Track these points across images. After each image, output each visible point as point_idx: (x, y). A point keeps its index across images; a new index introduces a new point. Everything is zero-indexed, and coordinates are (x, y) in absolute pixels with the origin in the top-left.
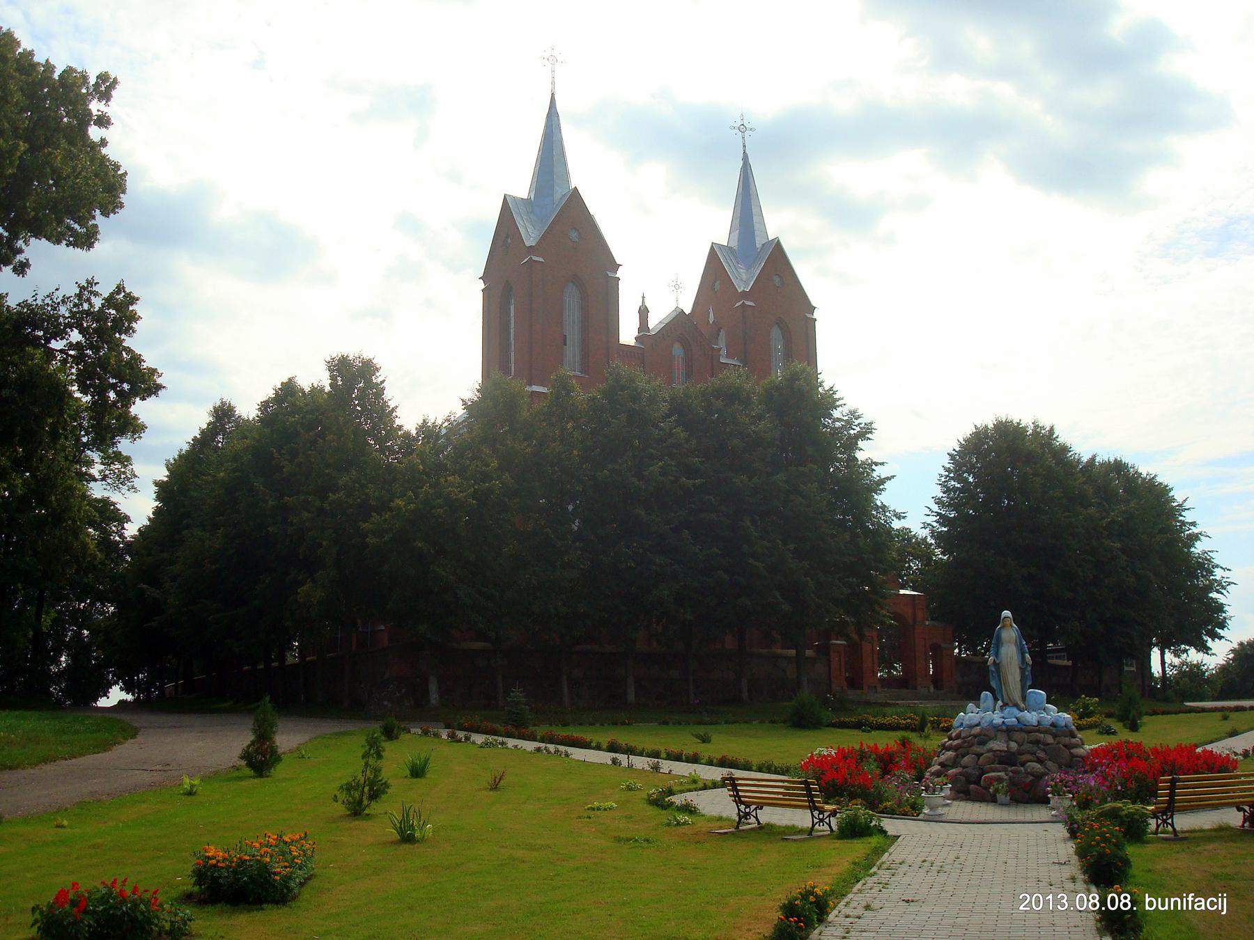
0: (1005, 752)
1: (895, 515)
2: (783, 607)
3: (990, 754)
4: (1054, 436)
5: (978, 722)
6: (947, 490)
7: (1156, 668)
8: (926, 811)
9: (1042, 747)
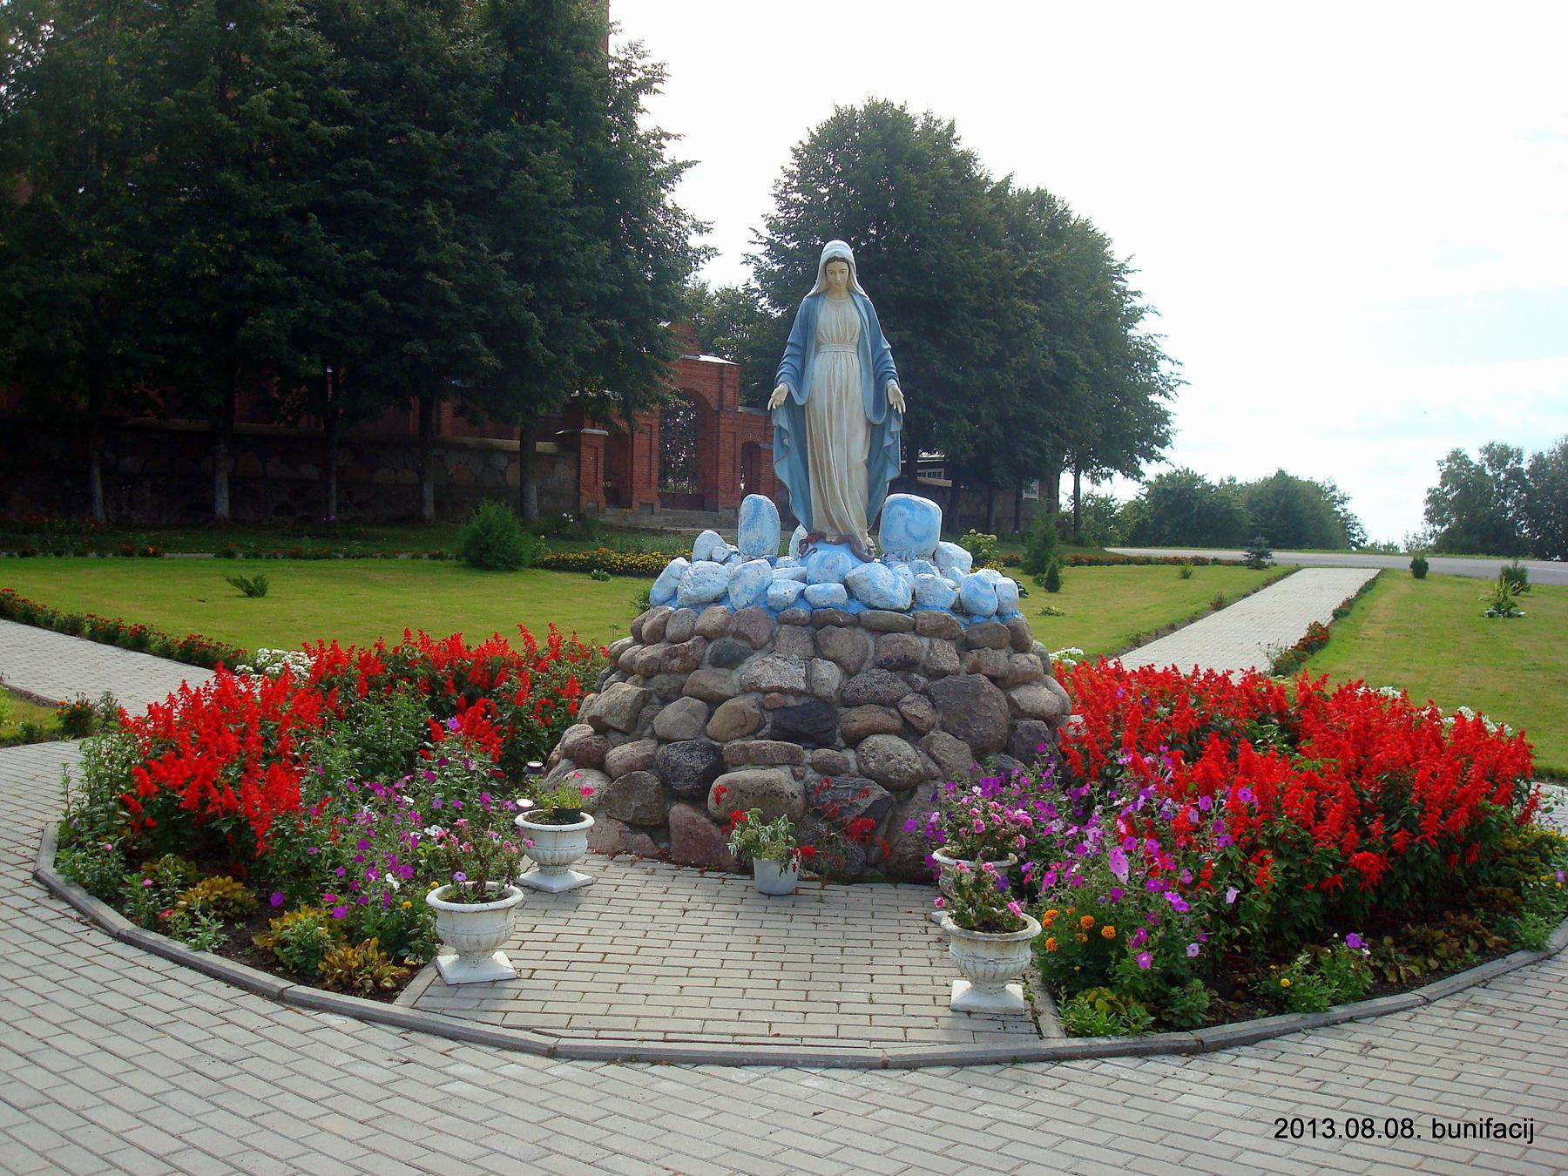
0: (798, 693)
1: (693, 226)
2: (485, 359)
3: (746, 702)
4: (955, 137)
5: (719, 590)
6: (788, 206)
7: (1065, 503)
8: (446, 959)
9: (922, 680)
